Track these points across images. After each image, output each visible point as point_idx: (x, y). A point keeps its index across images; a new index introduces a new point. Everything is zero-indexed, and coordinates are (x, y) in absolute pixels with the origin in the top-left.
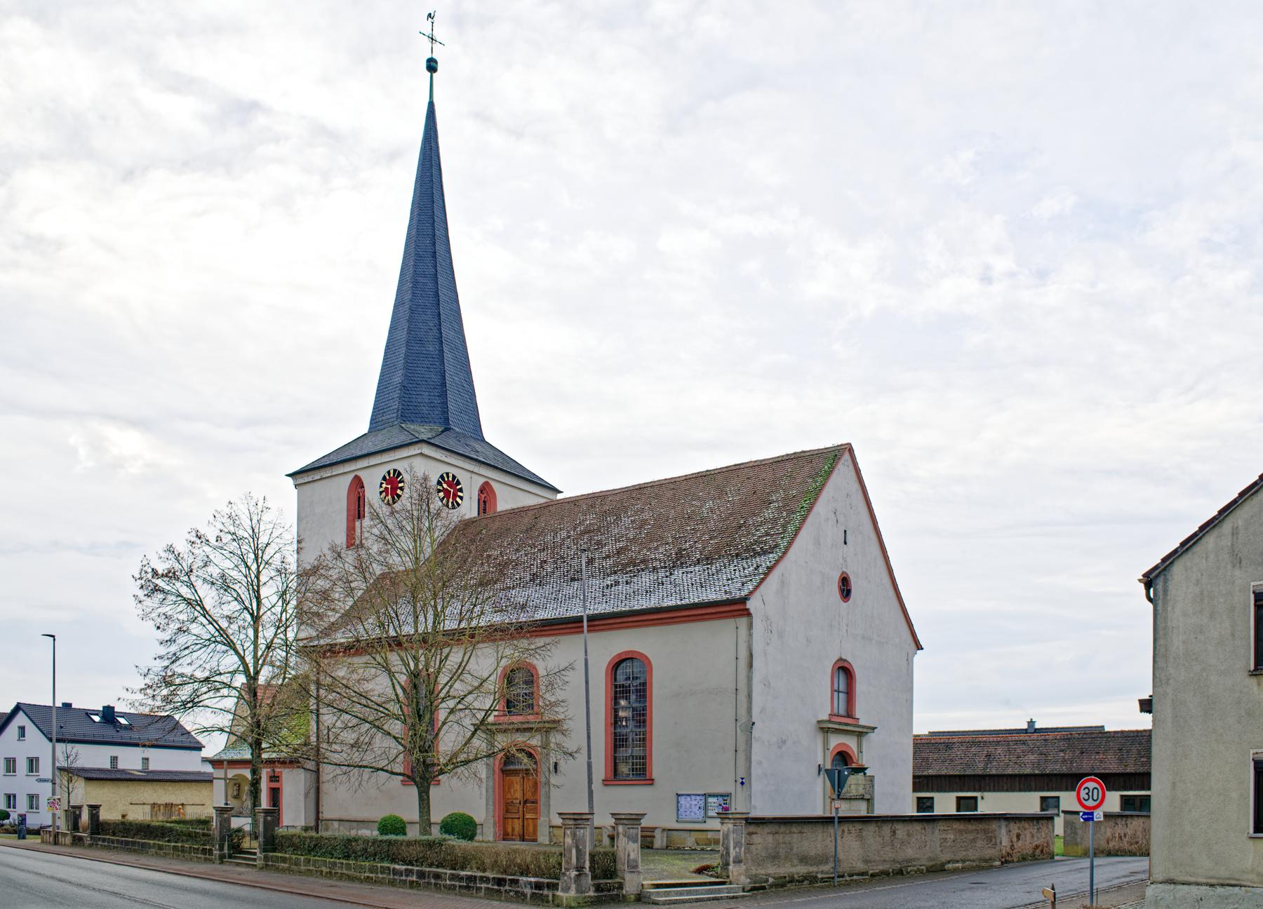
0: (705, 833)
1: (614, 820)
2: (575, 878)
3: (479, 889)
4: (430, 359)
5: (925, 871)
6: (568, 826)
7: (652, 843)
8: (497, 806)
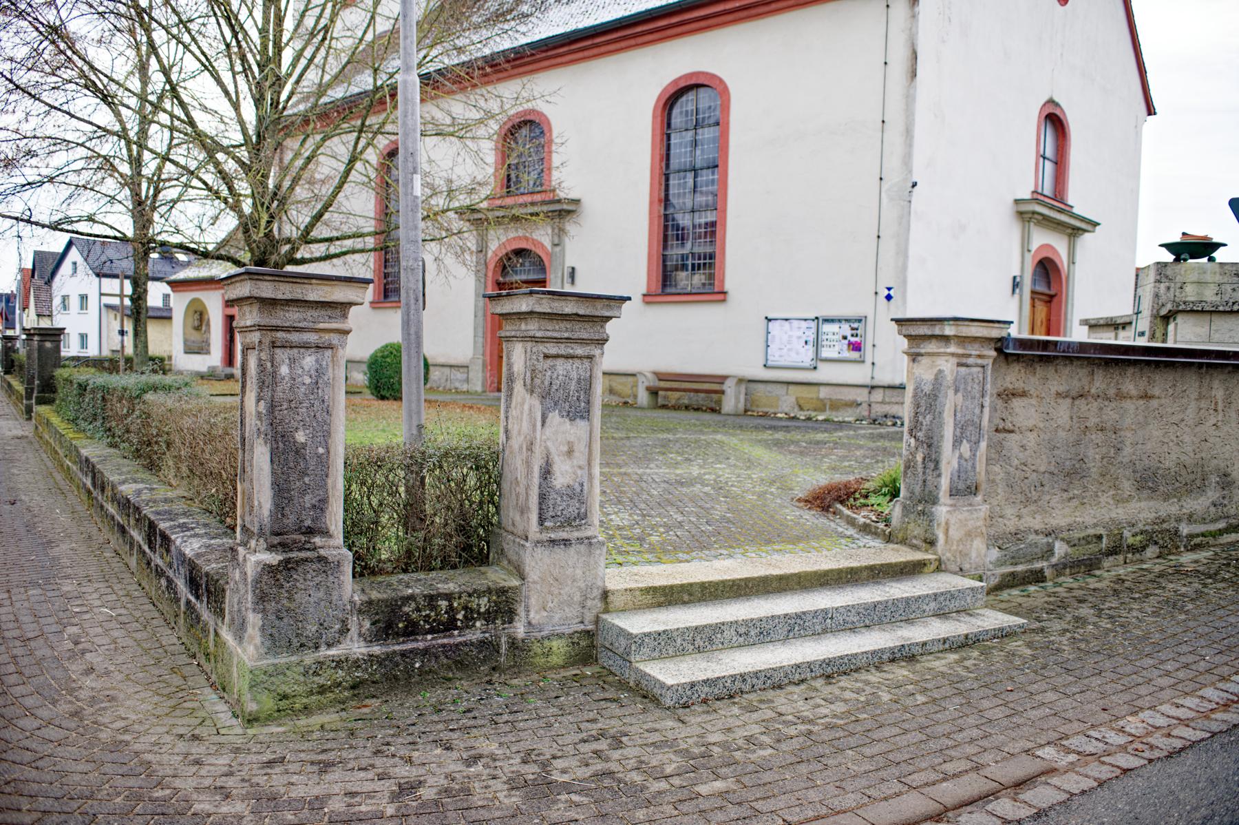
0: (815, 389)
2: (257, 581)
7: (719, 402)
8: (489, 340)
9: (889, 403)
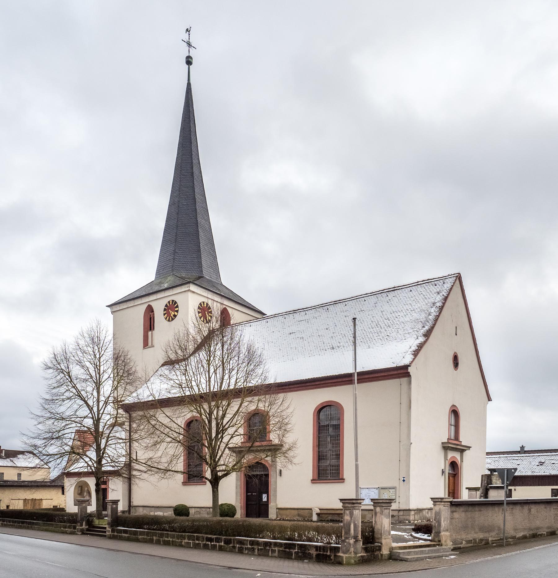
1: (342, 504)
3: (273, 551)
4: (191, 236)
5: (546, 535)
6: (347, 508)
9: (405, 515)
